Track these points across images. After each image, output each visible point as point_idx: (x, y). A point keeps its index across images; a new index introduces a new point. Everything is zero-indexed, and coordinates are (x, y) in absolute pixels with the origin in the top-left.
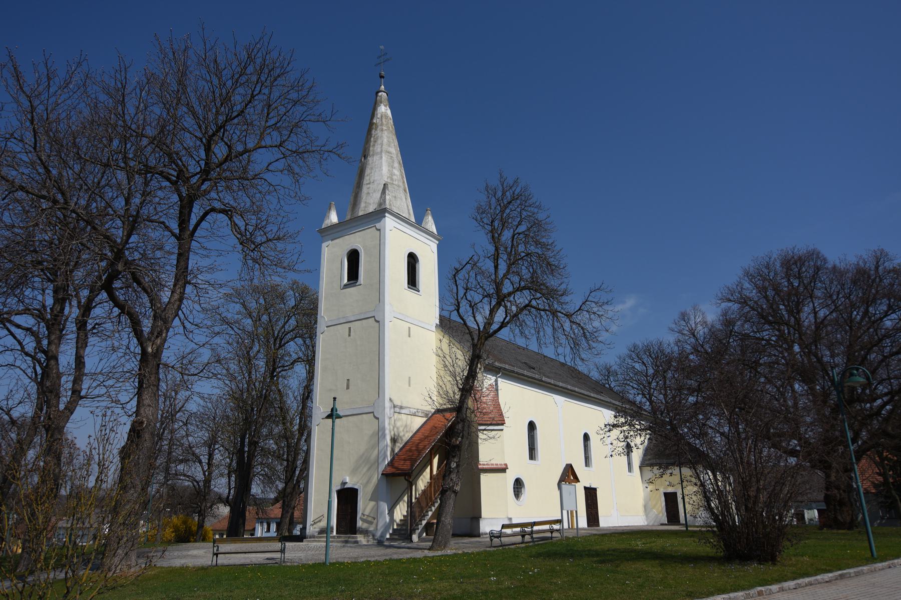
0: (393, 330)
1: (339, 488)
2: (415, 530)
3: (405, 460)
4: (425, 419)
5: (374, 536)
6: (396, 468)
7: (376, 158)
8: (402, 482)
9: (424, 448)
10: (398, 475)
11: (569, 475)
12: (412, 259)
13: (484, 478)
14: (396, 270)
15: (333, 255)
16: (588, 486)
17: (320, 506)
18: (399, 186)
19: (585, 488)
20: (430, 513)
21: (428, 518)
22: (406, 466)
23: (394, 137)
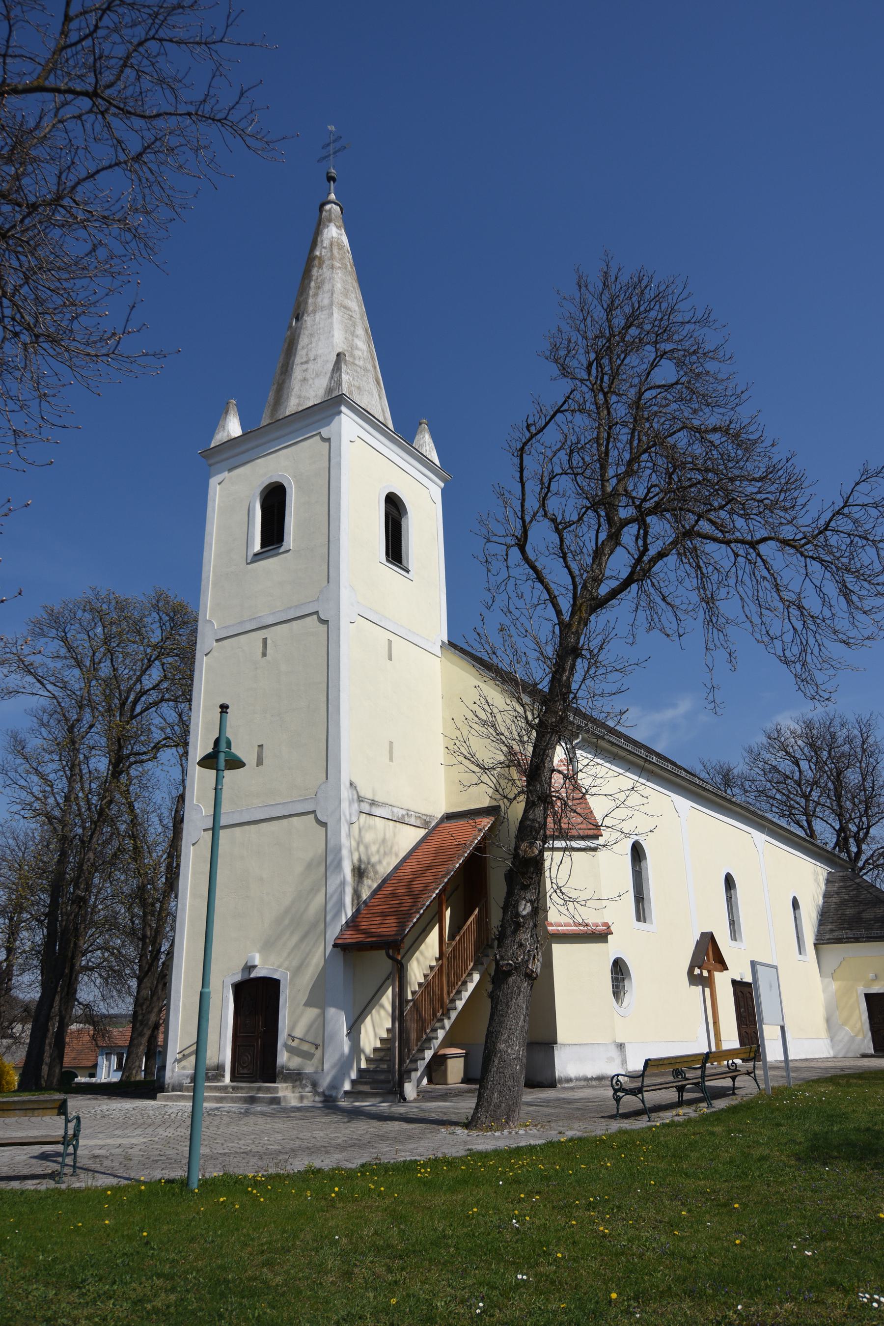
0: (355, 643)
1: (238, 978)
2: (409, 1072)
3: (383, 915)
4: (422, 832)
5: (315, 1085)
6: (365, 932)
7: (319, 316)
8: (381, 962)
9: (426, 888)
10: (370, 946)
11: (707, 956)
12: (394, 509)
13: (559, 950)
14: (363, 527)
15: (231, 502)
16: (738, 979)
17: (198, 1023)
18: (366, 370)
19: (734, 982)
20: (441, 1034)
21: (436, 1043)
22: (389, 927)
23: (356, 285)
